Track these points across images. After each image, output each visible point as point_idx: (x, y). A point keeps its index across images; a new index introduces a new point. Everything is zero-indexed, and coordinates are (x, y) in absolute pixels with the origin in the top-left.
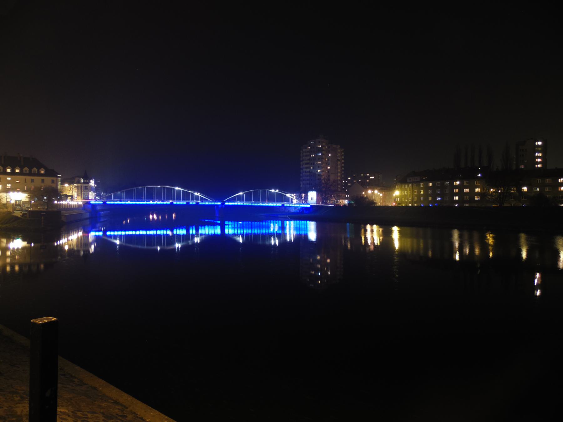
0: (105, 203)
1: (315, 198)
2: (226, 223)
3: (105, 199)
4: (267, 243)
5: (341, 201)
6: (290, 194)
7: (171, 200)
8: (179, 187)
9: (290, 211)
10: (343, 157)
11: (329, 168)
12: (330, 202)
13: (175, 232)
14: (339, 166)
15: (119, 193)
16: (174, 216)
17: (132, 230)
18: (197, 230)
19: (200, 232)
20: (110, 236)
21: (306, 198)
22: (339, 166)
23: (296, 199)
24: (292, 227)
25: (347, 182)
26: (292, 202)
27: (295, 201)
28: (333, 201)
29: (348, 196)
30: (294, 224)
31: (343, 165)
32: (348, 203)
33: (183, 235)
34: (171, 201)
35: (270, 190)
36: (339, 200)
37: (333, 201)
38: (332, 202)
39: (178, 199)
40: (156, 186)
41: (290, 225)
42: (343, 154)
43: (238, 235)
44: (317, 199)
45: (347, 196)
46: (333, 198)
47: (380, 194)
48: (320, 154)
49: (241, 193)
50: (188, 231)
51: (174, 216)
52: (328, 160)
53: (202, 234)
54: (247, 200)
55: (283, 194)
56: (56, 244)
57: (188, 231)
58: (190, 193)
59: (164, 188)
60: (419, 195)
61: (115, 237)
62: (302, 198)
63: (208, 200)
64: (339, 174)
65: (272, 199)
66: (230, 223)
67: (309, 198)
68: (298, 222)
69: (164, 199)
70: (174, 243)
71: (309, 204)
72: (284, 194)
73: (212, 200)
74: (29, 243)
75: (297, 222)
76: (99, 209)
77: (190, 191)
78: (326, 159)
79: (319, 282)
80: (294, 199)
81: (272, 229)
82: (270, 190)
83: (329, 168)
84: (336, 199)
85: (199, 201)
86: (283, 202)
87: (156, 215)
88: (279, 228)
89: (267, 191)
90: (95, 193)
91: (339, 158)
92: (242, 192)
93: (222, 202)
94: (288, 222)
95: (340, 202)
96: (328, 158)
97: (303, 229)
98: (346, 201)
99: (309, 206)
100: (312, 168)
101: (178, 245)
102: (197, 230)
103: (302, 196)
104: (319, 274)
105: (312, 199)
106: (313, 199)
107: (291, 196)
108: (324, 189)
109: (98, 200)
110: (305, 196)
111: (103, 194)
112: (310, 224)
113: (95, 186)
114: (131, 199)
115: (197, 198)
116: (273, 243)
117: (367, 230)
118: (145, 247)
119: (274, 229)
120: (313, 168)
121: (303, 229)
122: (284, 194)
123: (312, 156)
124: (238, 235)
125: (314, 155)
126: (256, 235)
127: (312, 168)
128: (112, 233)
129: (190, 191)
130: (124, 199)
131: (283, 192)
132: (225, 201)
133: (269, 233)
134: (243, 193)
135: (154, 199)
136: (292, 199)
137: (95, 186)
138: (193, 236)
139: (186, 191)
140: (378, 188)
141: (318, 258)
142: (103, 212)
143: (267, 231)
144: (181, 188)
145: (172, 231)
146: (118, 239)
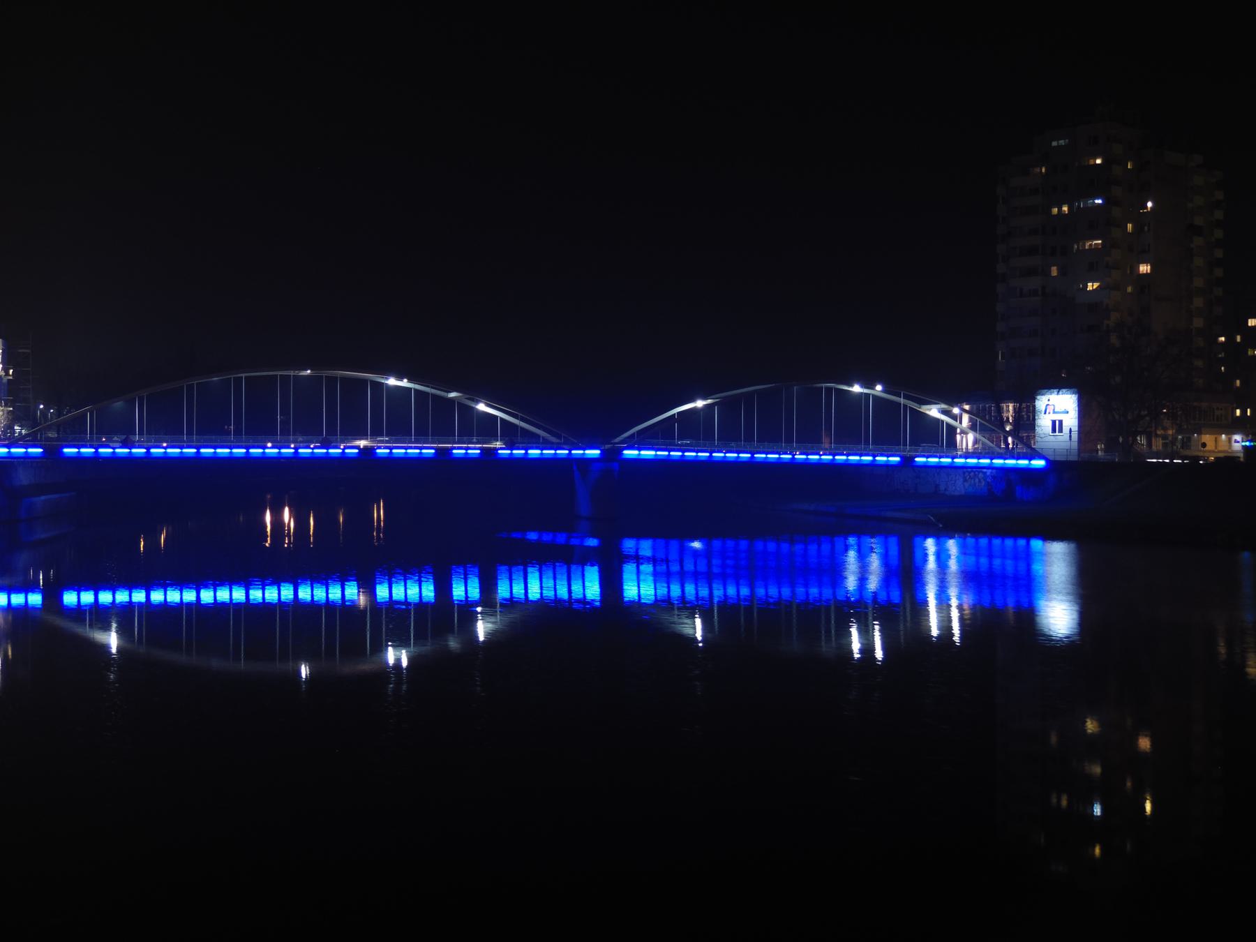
0: (53, 453)
1: (1071, 421)
2: (629, 545)
3: (53, 434)
4: (826, 648)
5: (1207, 438)
6: (944, 406)
7: (363, 435)
8: (400, 378)
9: (942, 488)
10: (1219, 215)
11: (1144, 269)
12: (1150, 444)
13: (382, 592)
14: (1198, 262)
15: (118, 405)
16: (379, 513)
17: (230, 581)
18: (488, 587)
19: (503, 591)
20: (79, 612)
21: (1026, 422)
22: (1198, 262)
23: (973, 427)
24: (953, 565)
25: (1239, 339)
26: (952, 444)
27: (967, 440)
28: (1164, 437)
29: (1244, 412)
30: (964, 551)
31: (1219, 253)
32: (1244, 447)
33: (421, 605)
34: (363, 443)
35: (846, 388)
36: (1200, 433)
37: (1164, 437)
38: (1158, 444)
39: (399, 431)
40: (292, 373)
41: (943, 556)
42: (1219, 195)
43: (689, 607)
44: (1080, 426)
45: (1238, 412)
46: (1167, 423)
47: (807, 594)
48: (1099, 201)
49: (700, 404)
50: (443, 589)
51: (379, 513)
52: (1138, 229)
53: (511, 602)
54: (729, 439)
55: (905, 406)
56: (700, 645)
57: (443, 589)
58: (452, 400)
59: (332, 381)
60: (868, 599)
61: (100, 616)
62: (1001, 423)
63: (538, 436)
64: (1198, 302)
65: (850, 437)
66: (646, 548)
67: (1044, 423)
68: (983, 542)
69: (332, 431)
70: (379, 649)
71: (1041, 457)
72: (914, 405)
73: (559, 437)
74: (406, 669)
75: (977, 543)
76: (25, 482)
77: (453, 395)
78: (1130, 226)
79: (1097, 851)
80: (963, 432)
81: (851, 583)
82: (846, 388)
83: (1144, 269)
84: (1180, 431)
85: (498, 444)
86: (867, 442)
87: (478, 637)
88: (890, 575)
89: (829, 390)
90: (6, 405)
91: (1198, 221)
92: (705, 398)
93: (607, 446)
94: (930, 544)
95: (1204, 445)
96: (1142, 221)
97: (1010, 583)
98: (1238, 437)
99: (1039, 463)
100: (1054, 271)
101: (398, 656)
102: (488, 587)
103: (1005, 415)
104: (1097, 810)
105: (1057, 426)
106: (1061, 430)
107: (944, 412)
108: (1118, 379)
109: (21, 437)
110: (1017, 412)
111: (44, 413)
112: (1043, 554)
113: (7, 374)
114: (173, 434)
115: (487, 427)
116: (391, 660)
117: (951, 606)
118: (243, 665)
119: (862, 580)
120: (1062, 272)
121: (1010, 583)
122: (914, 405)
123: (1055, 211)
124: (689, 607)
125: (1065, 209)
126: (771, 610)
127: (1054, 271)
128: (87, 597)
129: (453, 395)
130: (91, 433)
131: (906, 397)
132: (622, 442)
133: (837, 602)
134: (709, 401)
135: (285, 432)
136: (952, 430)
137: (7, 374)
138: (467, 611)
139: (434, 396)
140: (956, 536)
141: (1091, 726)
142: (43, 498)
143: (827, 593)
144: (410, 380)
145: (368, 587)
146: (114, 625)
